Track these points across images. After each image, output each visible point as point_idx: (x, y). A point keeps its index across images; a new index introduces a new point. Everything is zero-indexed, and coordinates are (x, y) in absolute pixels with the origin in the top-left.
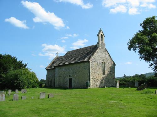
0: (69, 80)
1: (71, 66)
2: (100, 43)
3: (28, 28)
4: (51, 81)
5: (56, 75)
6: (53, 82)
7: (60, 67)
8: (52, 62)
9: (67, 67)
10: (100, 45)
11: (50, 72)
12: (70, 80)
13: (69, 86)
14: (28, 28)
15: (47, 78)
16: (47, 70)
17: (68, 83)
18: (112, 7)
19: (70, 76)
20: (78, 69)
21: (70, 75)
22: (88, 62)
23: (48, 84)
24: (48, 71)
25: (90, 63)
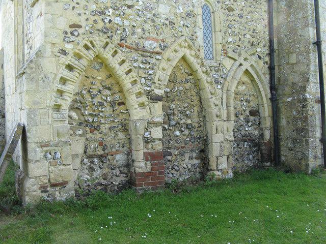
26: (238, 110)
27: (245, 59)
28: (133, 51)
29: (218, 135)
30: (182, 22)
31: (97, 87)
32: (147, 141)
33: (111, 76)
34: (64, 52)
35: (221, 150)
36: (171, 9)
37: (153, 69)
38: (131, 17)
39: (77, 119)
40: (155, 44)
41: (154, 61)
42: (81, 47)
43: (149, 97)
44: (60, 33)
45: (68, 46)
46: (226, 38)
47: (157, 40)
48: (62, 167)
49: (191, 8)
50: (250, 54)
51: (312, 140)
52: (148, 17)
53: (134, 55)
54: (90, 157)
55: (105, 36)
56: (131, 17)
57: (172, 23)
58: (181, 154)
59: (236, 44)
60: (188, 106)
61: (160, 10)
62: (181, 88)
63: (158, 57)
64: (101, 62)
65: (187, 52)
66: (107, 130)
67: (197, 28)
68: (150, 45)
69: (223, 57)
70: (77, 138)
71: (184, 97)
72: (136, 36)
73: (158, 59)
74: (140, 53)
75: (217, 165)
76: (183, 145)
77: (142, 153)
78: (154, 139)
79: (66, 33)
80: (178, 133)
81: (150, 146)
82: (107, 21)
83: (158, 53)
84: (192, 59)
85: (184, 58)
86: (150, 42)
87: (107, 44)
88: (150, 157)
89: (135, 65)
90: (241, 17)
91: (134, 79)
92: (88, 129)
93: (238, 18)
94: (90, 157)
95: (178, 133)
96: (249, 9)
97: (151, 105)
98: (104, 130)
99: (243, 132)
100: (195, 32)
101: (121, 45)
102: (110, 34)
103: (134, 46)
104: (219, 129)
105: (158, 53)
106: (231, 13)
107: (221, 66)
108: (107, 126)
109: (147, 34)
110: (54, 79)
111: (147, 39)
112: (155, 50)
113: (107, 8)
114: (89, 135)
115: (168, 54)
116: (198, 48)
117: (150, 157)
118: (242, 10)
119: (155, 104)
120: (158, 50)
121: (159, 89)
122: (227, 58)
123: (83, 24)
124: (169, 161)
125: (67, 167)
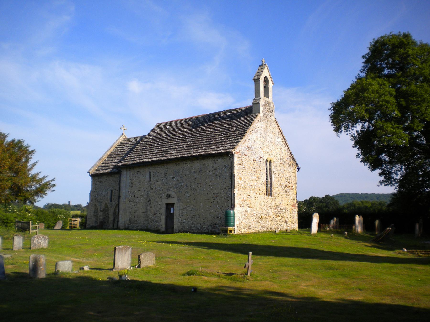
0: (164, 206)
1: (172, 167)
2: (262, 102)
3: (396, 197)
4: (106, 211)
5: (123, 191)
6: (111, 212)
7: (136, 170)
8: (108, 153)
9: (161, 170)
10: (261, 108)
11: (101, 182)
12: (169, 206)
13: (164, 226)
14: (396, 197)
15: (92, 199)
16: (93, 176)
17: (163, 218)
18: (127, 174)
19: (169, 196)
20: (195, 175)
21: (170, 193)
22: (229, 155)
23: (94, 219)
24: (97, 178)
25: (236, 159)
32: (100, 219)
64: (95, 205)
84: (107, 203)
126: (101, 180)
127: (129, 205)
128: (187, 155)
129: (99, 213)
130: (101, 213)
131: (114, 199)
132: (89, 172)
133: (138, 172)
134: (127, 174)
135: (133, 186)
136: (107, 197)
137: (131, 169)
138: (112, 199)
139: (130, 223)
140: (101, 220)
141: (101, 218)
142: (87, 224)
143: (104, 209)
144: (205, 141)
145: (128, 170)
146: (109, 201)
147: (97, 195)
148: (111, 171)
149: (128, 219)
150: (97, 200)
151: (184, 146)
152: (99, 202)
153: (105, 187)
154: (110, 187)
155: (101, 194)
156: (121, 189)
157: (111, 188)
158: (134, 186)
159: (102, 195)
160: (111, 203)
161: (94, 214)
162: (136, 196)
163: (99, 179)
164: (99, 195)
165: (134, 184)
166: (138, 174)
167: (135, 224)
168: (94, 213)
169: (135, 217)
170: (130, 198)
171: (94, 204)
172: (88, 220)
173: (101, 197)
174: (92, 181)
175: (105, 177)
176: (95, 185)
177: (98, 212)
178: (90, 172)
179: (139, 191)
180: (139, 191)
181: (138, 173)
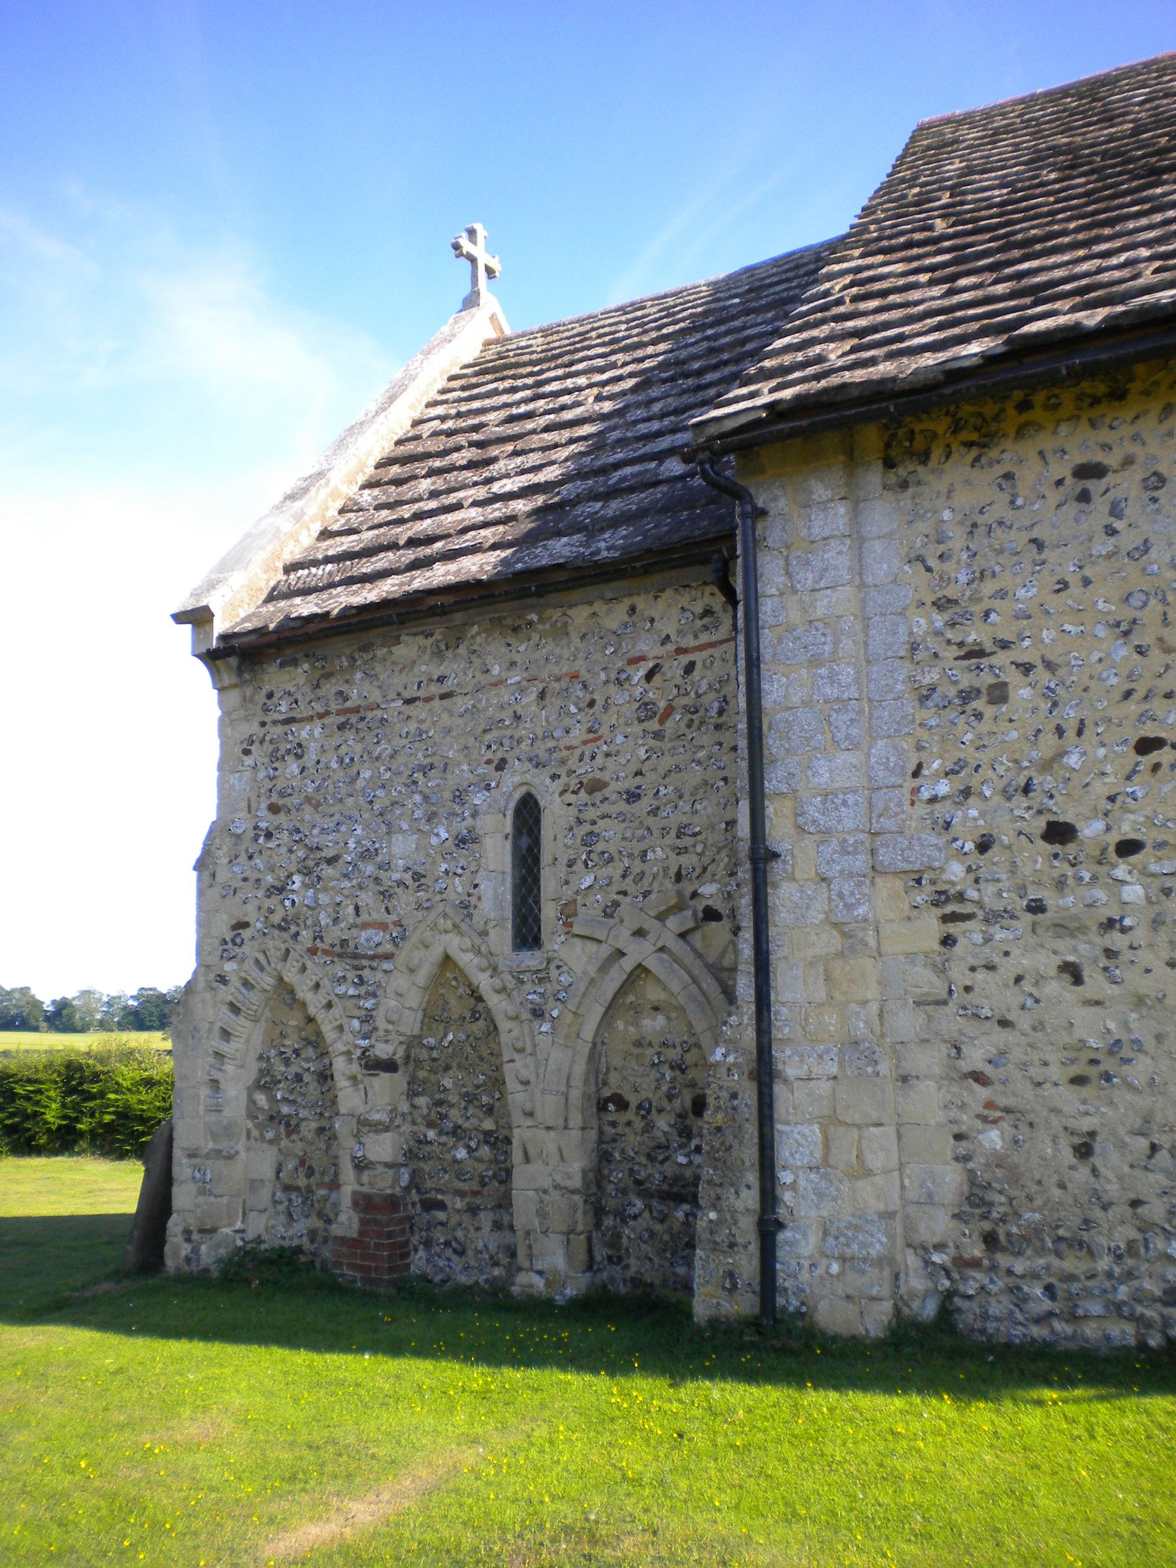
18: (858, 539)
26: (644, 1095)
27: (640, 933)
28: (336, 959)
29: (529, 1167)
30: (444, 867)
31: (292, 1042)
32: (361, 1165)
33: (1097, 878)
34: (222, 979)
35: (542, 1214)
36: (419, 839)
37: (374, 995)
38: (332, 884)
39: (266, 1107)
40: (379, 936)
41: (379, 976)
42: (249, 965)
43: (363, 1062)
44: (217, 942)
45: (229, 967)
46: (573, 879)
47: (383, 926)
48: (212, 1199)
49: (469, 821)
50: (653, 913)
51: (713, 1215)
52: (368, 873)
53: (339, 969)
54: (287, 1188)
55: (285, 935)
56: (332, 884)
57: (417, 876)
58: (473, 1210)
59: (616, 887)
60: (484, 1084)
61: (395, 850)
62: (462, 1036)
63: (386, 966)
64: (286, 993)
65: (454, 944)
66: (312, 1134)
67: (482, 873)
68: (368, 939)
69: (563, 938)
70: (265, 1145)
71: (473, 1057)
72: (343, 925)
73: (385, 971)
74: (348, 961)
75: (531, 1257)
76: (476, 1188)
77: (349, 1192)
78: (371, 1163)
79: (225, 942)
80: (461, 1154)
81: (365, 1178)
82: (287, 903)
83: (388, 957)
84: (466, 960)
85: (447, 959)
86: (370, 932)
87: (288, 951)
88: (364, 1203)
89: (341, 990)
90: (633, 797)
91: (338, 1023)
92: (282, 1129)
93: (622, 806)
94: (287, 1188)
95: (461, 1154)
96: (667, 762)
97: (367, 1080)
98: (306, 1133)
99: (668, 1168)
100: (476, 886)
101: (313, 951)
102: (293, 928)
103: (337, 949)
104: (532, 1152)
105: (388, 957)
106: (598, 796)
107: (553, 966)
108: (314, 1125)
109: (364, 917)
110: (210, 1031)
111: (365, 926)
112: (380, 950)
113: (290, 876)
114: (284, 1143)
115: (408, 953)
116: (481, 927)
117: (364, 1203)
118: (639, 773)
119: (373, 1079)
120: (388, 947)
121: (387, 1041)
122: (575, 940)
123: (251, 918)
124: (442, 1224)
125: (219, 1200)
126: (359, 690)
127: (941, 970)
128: (942, 356)
129: (342, 1082)
130: (382, 1083)
131: (568, 913)
132: (198, 618)
133: (1090, 471)
134: (858, 539)
135: (999, 694)
136: (459, 886)
137: (924, 457)
138: (549, 912)
139: (990, 1240)
140: (383, 1183)
141: (382, 1148)
142: (175, 1225)
143: (413, 1042)
144: (529, 369)
145: (873, 477)
146: (502, 938)
147: (306, 872)
148: (504, 562)
149: (952, 1179)
150: (306, 935)
151: (1039, 210)
152: (345, 952)
153: (426, 769)
154: (501, 766)
155: (366, 855)
156: (772, 743)
157: (512, 783)
158: (1022, 693)
159: (386, 866)
160: (531, 959)
161: (261, 1099)
162: (1090, 830)
163: (330, 689)
164: (327, 871)
165: (1026, 651)
166: (1100, 506)
167: (1104, 1263)
168: (265, 1082)
169: (1084, 1151)
170: (956, 871)
171: (267, 981)
172: (182, 1168)
173: (366, 898)
174: (227, 722)
175: (408, 648)
176: (275, 757)
177: (325, 1077)
178: (215, 603)
179: (1146, 746)
180: (1146, 746)
181: (1084, 497)
